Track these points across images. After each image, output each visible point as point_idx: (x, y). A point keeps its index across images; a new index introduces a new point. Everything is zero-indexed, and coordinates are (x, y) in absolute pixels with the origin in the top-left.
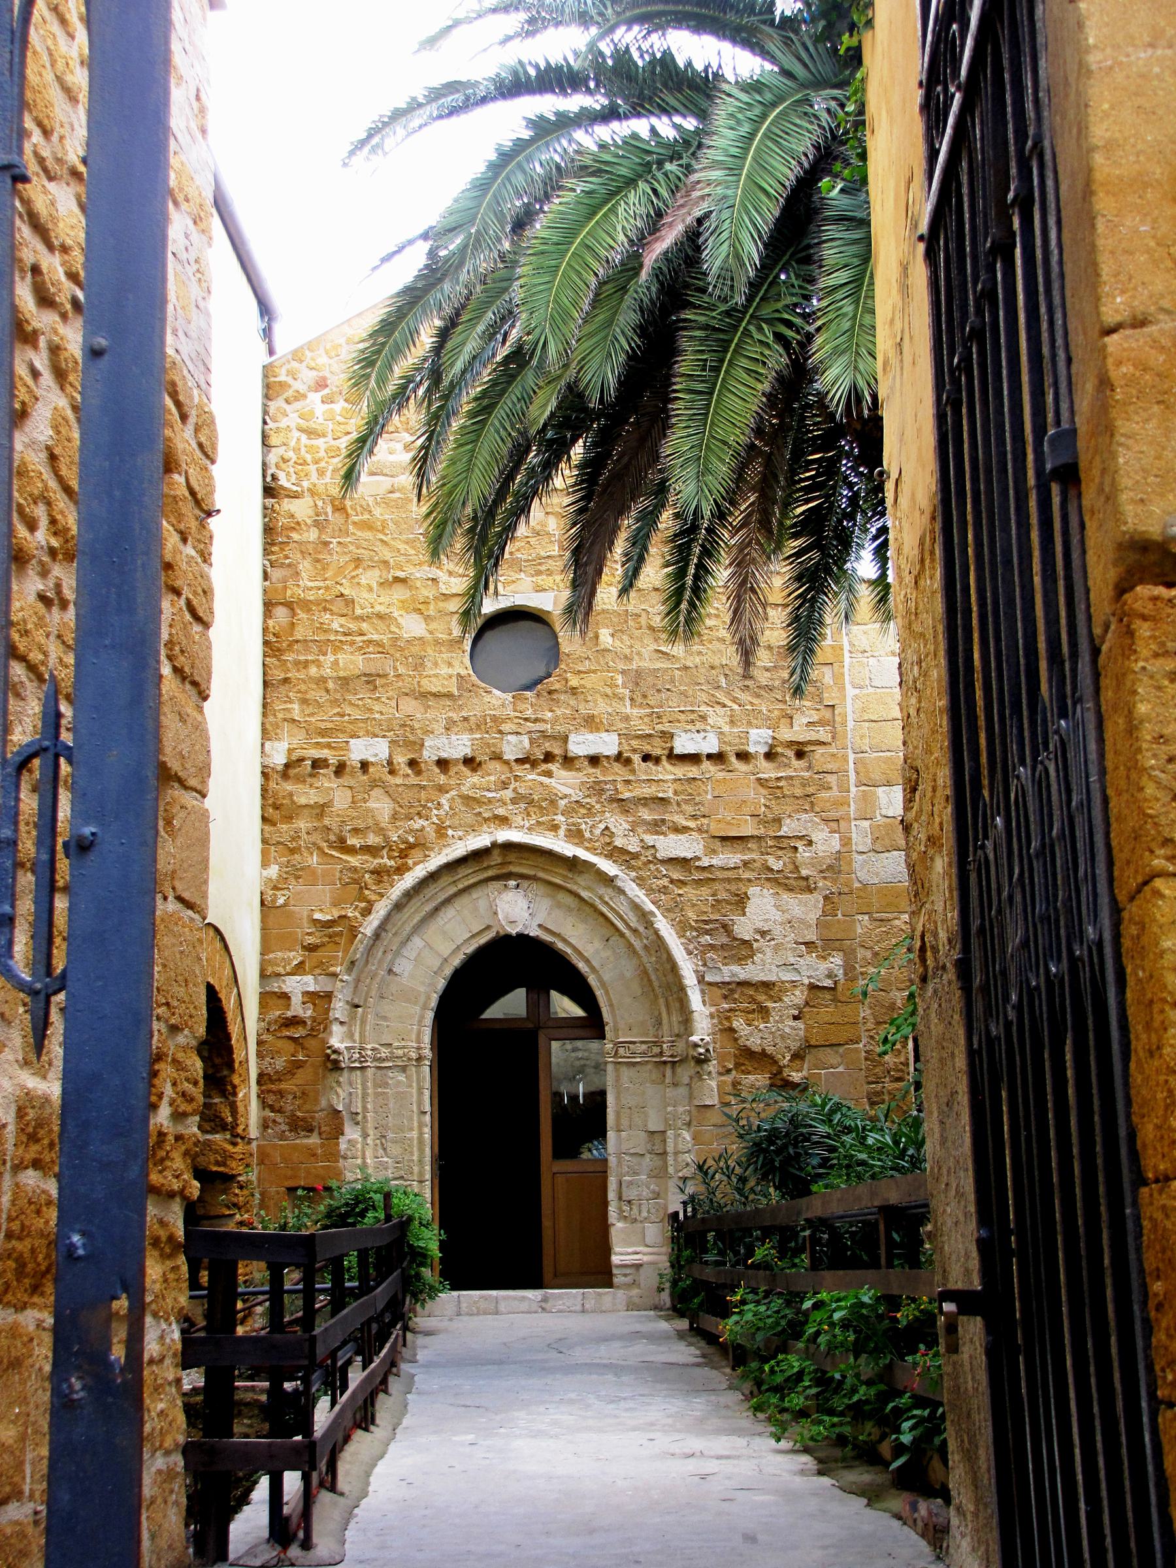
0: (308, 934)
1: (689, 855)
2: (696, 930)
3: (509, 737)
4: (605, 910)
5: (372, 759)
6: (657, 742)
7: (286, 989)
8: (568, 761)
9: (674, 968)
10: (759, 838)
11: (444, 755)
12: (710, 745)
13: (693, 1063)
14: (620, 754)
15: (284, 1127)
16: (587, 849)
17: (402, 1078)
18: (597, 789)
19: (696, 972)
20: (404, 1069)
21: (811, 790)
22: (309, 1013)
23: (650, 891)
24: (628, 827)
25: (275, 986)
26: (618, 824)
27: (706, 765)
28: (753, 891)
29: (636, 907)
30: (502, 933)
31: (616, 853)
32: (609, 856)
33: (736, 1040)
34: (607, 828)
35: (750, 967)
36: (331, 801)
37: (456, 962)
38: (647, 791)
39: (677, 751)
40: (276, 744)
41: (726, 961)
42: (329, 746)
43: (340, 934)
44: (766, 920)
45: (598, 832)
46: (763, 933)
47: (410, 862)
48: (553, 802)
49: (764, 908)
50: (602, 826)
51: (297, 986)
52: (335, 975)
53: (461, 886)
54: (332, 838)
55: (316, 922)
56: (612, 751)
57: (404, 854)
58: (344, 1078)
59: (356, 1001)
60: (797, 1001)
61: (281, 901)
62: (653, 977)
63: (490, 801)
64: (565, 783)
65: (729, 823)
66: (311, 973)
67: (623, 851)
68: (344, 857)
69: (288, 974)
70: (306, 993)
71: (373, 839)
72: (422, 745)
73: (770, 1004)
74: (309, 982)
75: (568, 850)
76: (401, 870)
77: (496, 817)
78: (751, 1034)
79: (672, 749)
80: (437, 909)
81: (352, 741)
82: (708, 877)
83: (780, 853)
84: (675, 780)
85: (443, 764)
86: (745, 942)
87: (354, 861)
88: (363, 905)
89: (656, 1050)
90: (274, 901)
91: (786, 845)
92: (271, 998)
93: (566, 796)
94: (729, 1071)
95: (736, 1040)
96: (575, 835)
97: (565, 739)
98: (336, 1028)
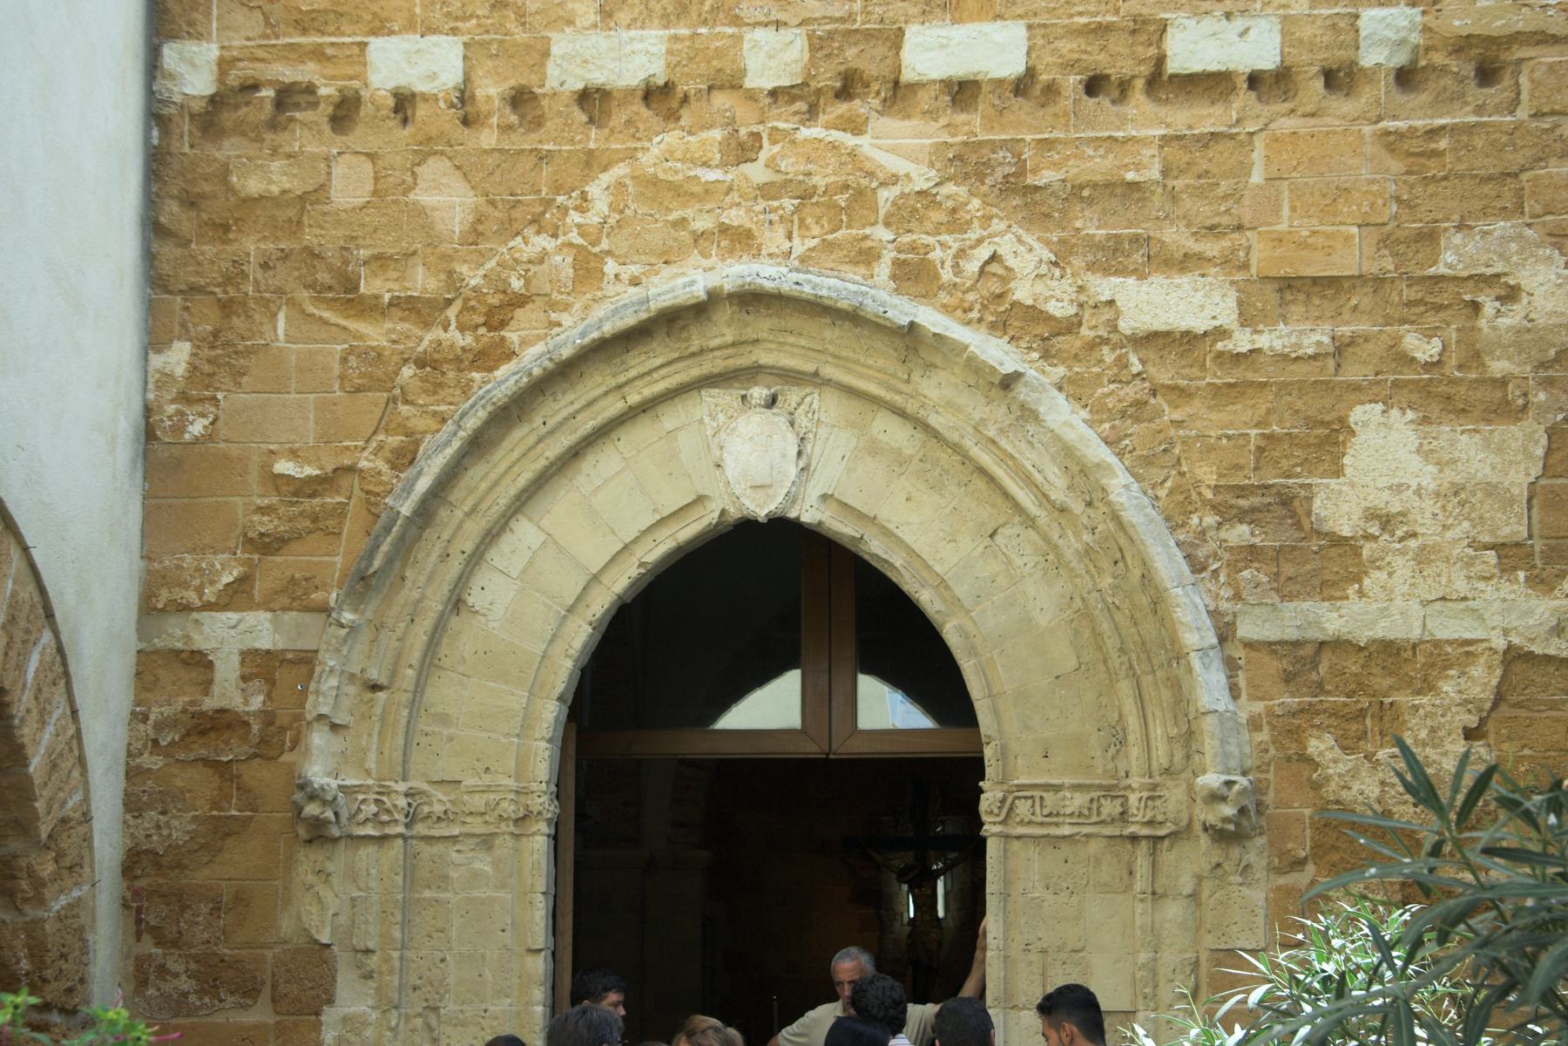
0: (261, 510)
1: (1200, 324)
2: (1215, 508)
3: (760, 34)
4: (986, 459)
5: (420, 87)
6: (1119, 44)
7: (200, 643)
8: (899, 93)
9: (1158, 604)
10: (1379, 282)
11: (598, 78)
12: (1259, 48)
13: (1204, 841)
14: (1031, 73)
15: (185, 984)
16: (946, 309)
17: (483, 864)
18: (965, 163)
19: (1214, 614)
20: (486, 842)
21: (1515, 159)
22: (257, 702)
23: (1098, 414)
24: (1049, 256)
25: (174, 633)
26: (1023, 253)
27: (1244, 99)
28: (1363, 414)
29: (1067, 454)
30: (734, 514)
31: (1014, 319)
32: (999, 327)
33: (1316, 786)
34: (994, 258)
35: (1353, 605)
36: (323, 188)
37: (620, 582)
38: (1098, 165)
39: (1173, 66)
40: (191, 47)
41: (1286, 589)
42: (318, 54)
43: (340, 511)
44: (1398, 489)
45: (972, 267)
46: (1386, 521)
47: (512, 336)
48: (862, 197)
49: (1387, 459)
50: (984, 253)
51: (230, 635)
52: (324, 609)
53: (634, 398)
54: (324, 277)
55: (279, 482)
56: (1013, 66)
57: (497, 319)
58: (338, 861)
59: (374, 674)
60: (1475, 691)
61: (197, 428)
62: (1105, 626)
63: (709, 190)
64: (898, 149)
65: (1303, 245)
66: (266, 605)
67: (1034, 314)
68: (352, 325)
69: (208, 607)
70: (248, 655)
71: (423, 282)
72: (546, 54)
73: (1403, 698)
74: (261, 629)
75: (902, 310)
76: (489, 357)
77: (724, 229)
78: (1354, 773)
79: (1161, 60)
80: (575, 454)
81: (375, 43)
82: (1241, 376)
83: (1433, 319)
84: (1166, 140)
85: (592, 100)
86: (1338, 541)
87: (375, 334)
88: (395, 440)
89: (1110, 808)
90: (180, 429)
91: (1454, 299)
92: (165, 665)
93: (894, 180)
94: (1300, 863)
95: (1316, 786)
96: (914, 274)
97: (896, 40)
98: (318, 738)
